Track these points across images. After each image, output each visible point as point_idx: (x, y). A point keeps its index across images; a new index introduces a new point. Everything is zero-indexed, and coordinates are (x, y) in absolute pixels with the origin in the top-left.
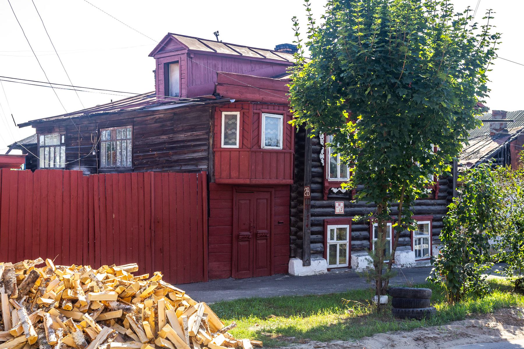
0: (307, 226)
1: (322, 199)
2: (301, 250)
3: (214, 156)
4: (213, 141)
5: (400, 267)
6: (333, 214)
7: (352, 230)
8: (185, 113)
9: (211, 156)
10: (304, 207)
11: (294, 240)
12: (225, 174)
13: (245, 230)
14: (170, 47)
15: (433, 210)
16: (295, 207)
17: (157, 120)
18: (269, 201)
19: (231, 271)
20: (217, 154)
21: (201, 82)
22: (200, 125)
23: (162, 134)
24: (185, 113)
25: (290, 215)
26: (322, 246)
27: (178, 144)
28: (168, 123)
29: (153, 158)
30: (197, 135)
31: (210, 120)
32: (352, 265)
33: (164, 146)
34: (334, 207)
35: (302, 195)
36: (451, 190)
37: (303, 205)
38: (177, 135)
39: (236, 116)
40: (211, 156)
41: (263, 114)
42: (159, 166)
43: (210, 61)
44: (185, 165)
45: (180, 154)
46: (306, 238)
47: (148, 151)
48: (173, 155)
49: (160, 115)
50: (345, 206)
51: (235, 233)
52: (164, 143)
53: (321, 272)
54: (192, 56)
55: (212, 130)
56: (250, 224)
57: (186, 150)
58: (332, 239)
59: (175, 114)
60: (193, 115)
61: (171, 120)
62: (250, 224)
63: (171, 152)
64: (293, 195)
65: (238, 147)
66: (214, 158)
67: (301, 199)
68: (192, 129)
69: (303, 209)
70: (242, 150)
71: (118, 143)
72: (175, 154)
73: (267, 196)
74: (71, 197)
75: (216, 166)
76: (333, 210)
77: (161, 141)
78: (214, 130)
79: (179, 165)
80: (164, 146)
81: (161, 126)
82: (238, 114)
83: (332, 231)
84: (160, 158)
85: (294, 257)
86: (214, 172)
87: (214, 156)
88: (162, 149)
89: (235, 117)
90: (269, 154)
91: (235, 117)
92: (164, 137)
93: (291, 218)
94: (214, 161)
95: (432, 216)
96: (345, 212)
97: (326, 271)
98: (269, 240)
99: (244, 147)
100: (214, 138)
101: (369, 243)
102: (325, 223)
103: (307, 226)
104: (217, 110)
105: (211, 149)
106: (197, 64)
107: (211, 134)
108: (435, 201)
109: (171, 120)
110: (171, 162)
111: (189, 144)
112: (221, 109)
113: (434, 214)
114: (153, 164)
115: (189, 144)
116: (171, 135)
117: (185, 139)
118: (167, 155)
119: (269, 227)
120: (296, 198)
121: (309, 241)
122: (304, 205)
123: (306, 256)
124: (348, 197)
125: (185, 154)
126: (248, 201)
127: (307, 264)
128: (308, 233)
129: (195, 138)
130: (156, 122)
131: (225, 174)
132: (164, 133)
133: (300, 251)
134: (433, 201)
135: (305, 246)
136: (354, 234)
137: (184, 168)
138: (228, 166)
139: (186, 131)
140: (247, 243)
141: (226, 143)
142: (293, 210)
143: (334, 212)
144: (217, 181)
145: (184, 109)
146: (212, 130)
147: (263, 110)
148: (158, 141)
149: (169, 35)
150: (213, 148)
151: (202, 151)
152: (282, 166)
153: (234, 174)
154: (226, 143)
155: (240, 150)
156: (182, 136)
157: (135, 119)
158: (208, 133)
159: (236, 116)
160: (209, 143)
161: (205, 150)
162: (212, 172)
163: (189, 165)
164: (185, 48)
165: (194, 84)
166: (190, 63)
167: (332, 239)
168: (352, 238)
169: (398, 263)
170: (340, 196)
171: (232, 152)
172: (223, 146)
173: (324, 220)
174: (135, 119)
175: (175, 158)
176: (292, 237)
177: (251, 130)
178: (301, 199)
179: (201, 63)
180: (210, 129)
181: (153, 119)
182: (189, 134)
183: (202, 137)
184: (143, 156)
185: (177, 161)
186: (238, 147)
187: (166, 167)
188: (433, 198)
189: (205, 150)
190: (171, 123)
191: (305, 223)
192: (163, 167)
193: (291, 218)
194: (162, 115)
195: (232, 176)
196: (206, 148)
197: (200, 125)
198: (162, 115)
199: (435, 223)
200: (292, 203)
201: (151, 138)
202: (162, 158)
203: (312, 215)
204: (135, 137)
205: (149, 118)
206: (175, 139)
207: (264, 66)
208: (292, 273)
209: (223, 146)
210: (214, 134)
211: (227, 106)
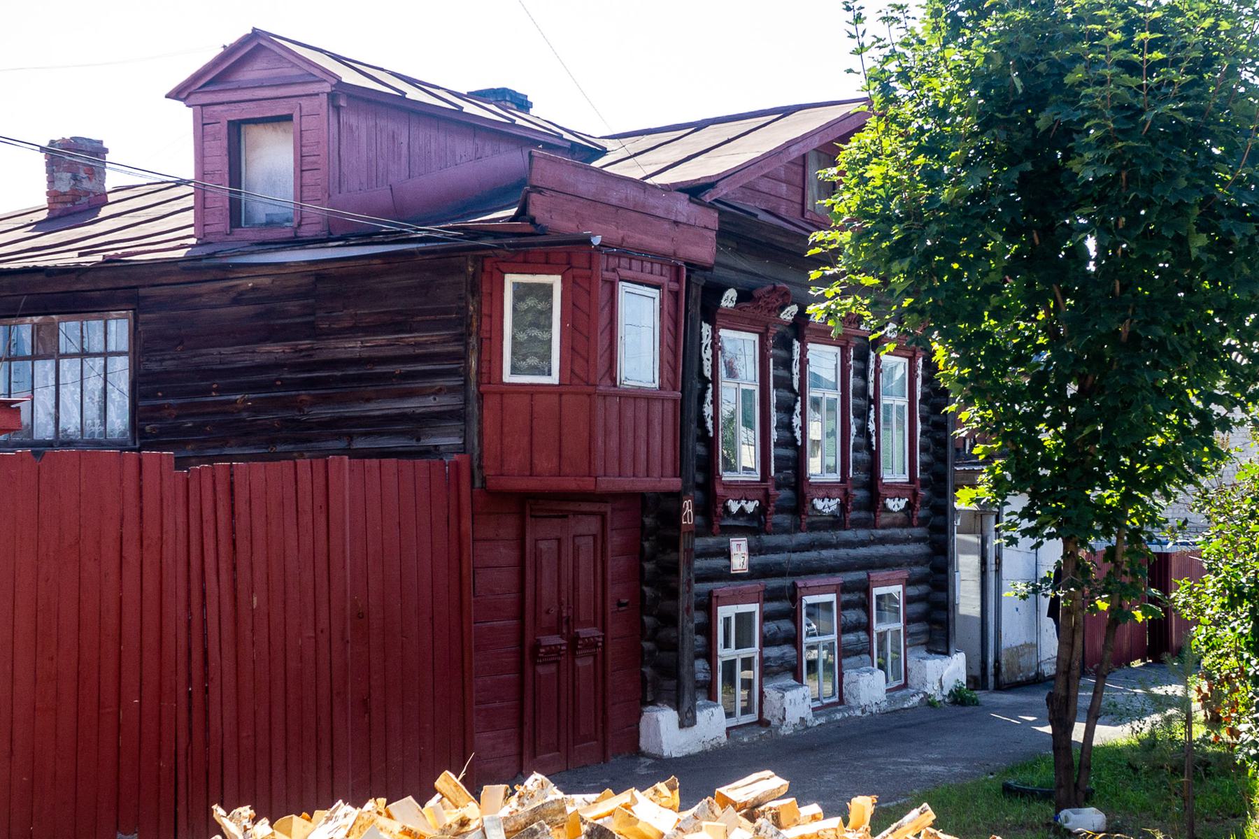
0: (688, 610)
1: (798, 528)
2: (674, 682)
3: (481, 408)
4: (479, 361)
5: (859, 713)
6: (725, 575)
7: (766, 617)
11: (651, 653)
13: (551, 631)
14: (255, 71)
15: (907, 557)
16: (652, 557)
17: (240, 294)
18: (599, 542)
19: (521, 754)
20: (491, 402)
23: (264, 340)
26: (707, 666)
28: (293, 306)
29: (225, 413)
30: (417, 344)
31: (470, 297)
32: (765, 716)
34: (727, 555)
36: (940, 501)
37: (677, 550)
38: (333, 343)
39: (548, 289)
40: (473, 408)
41: (621, 284)
43: (382, 123)
46: (687, 645)
47: (207, 392)
50: (752, 551)
51: (529, 639)
52: (277, 366)
53: (714, 743)
54: (343, 103)
55: (474, 329)
56: (560, 612)
58: (726, 645)
61: (305, 295)
62: (560, 612)
63: (304, 395)
69: (677, 563)
70: (571, 389)
72: (325, 400)
73: (592, 525)
74: (145, 543)
75: (486, 441)
77: (258, 359)
79: (339, 437)
80: (274, 376)
81: (258, 316)
83: (727, 620)
85: (653, 703)
86: (481, 452)
87: (481, 408)
88: (269, 386)
92: (275, 350)
93: (646, 589)
94: (480, 422)
96: (751, 566)
97: (724, 739)
98: (599, 658)
99: (576, 381)
101: (794, 653)
102: (714, 600)
103: (688, 610)
105: (473, 387)
106: (351, 127)
107: (473, 341)
108: (910, 530)
109: (305, 295)
110: (309, 426)
111: (379, 369)
113: (909, 565)
114: (226, 432)
115: (379, 369)
116: (305, 344)
117: (366, 354)
118: (286, 404)
119: (599, 622)
121: (691, 655)
122: (682, 549)
123: (687, 697)
125: (368, 400)
126: (554, 544)
127: (687, 721)
128: (690, 631)
129: (410, 351)
130: (236, 301)
132: (272, 335)
133: (670, 684)
134: (905, 532)
135: (684, 671)
136: (772, 626)
138: (526, 439)
140: (553, 668)
142: (648, 566)
143: (729, 567)
144: (492, 483)
145: (366, 262)
146: (473, 329)
147: (623, 273)
148: (246, 360)
149: (256, 34)
150: (479, 384)
151: (438, 392)
152: (658, 438)
153: (545, 463)
155: (564, 389)
156: (353, 347)
157: (142, 292)
158: (462, 338)
160: (467, 368)
161: (451, 390)
164: (324, 76)
165: (344, 189)
166: (333, 120)
167: (726, 645)
168: (766, 642)
169: (853, 703)
170: (741, 522)
171: (537, 397)
172: (508, 378)
173: (710, 593)
174: (142, 292)
176: (647, 645)
177: (592, 334)
179: (360, 124)
180: (469, 325)
181: (223, 290)
182: (381, 339)
183: (437, 349)
184: (181, 406)
187: (286, 441)
188: (907, 523)
191: (683, 601)
192: (272, 442)
193: (646, 589)
194: (267, 281)
199: (846, 597)
200: (646, 544)
201: (214, 351)
203: (700, 579)
204: (141, 349)
205: (206, 287)
208: (655, 751)
209: (508, 378)
211: (521, 258)
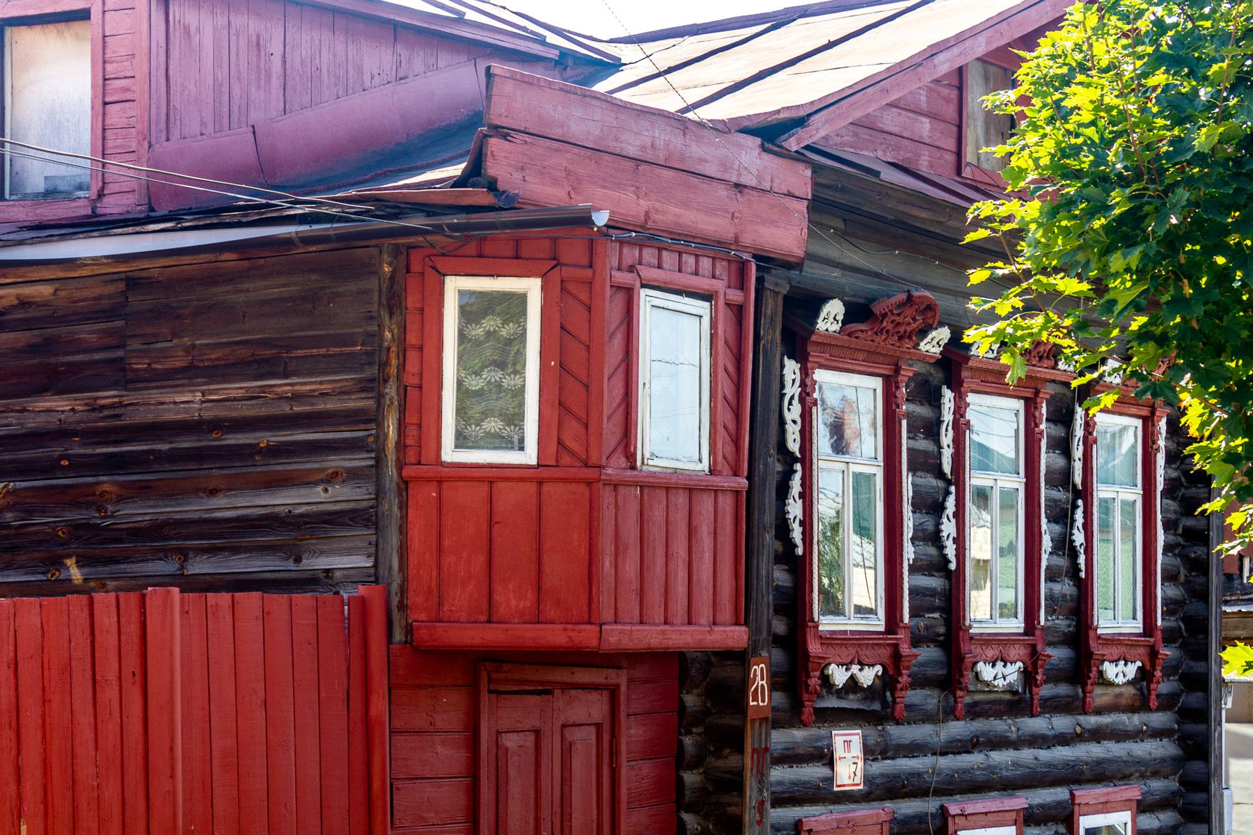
8: (231, 278)
9: (391, 505)
10: (748, 761)
12: (461, 598)
15: (1139, 762)
20: (425, 495)
21: (203, 124)
22: (318, 342)
23: (41, 390)
24: (213, 278)
25: (681, 805)
27: (159, 438)
28: (88, 333)
30: (296, 397)
33: (57, 451)
35: (740, 706)
36: (1198, 667)
37: (741, 751)
38: (155, 395)
39: (522, 299)
40: (391, 505)
42: (22, 558)
43: (239, 20)
44: (212, 551)
45: (172, 493)
48: (121, 499)
49: (27, 291)
50: (870, 753)
52: (62, 434)
55: (393, 371)
57: (217, 474)
59: (133, 283)
60: (273, 288)
61: (109, 314)
63: (107, 483)
64: (691, 700)
65: (533, 461)
66: (404, 517)
67: (730, 720)
68: (260, 362)
71: (995, 423)
72: (142, 491)
75: (413, 560)
76: (825, 771)
77: (32, 423)
78: (402, 367)
79: (165, 554)
80: (57, 451)
81: (32, 349)
82: (532, 288)
84: (30, 512)
86: (403, 590)
87: (404, 506)
89: (514, 305)
90: (662, 494)
91: (514, 305)
92: (59, 407)
94: (403, 530)
95: (1134, 791)
96: (868, 779)
99: (566, 459)
100: (402, 411)
104: (416, 267)
105: (391, 470)
107: (391, 390)
109: (109, 314)
112: (441, 263)
113: (1143, 776)
116: (108, 396)
117: (207, 415)
118: (80, 497)
120: (700, 717)
122: (748, 750)
124: (876, 706)
125: (213, 493)
126: (531, 738)
129: (286, 408)
131: (461, 598)
132: (55, 381)
134: (1136, 720)
137: (200, 566)
138: (480, 560)
139: (218, 372)
141: (462, 441)
142: (691, 778)
143: (830, 780)
146: (393, 372)
150: (400, 466)
152: (708, 557)
153: (512, 599)
154: (462, 441)
155: (545, 473)
156: (188, 401)
158: (372, 386)
159: (522, 299)
160: (381, 438)
161: (353, 475)
162: (395, 587)
163: (235, 550)
165: (175, 134)
170: (851, 702)
172: (450, 453)
175: (139, 512)
177: (593, 381)
178: (730, 720)
180: (384, 365)
182: (235, 388)
183: (331, 405)
185: (156, 536)
186: (533, 461)
189: (353, 475)
190: (110, 333)
193: (687, 817)
195: (502, 610)
196: (358, 461)
197: (318, 342)
198: (46, 290)
200: (688, 741)
202: (44, 512)
206: (143, 416)
207: (444, 59)
209: (450, 453)
210: (403, 392)
211: (471, 248)
